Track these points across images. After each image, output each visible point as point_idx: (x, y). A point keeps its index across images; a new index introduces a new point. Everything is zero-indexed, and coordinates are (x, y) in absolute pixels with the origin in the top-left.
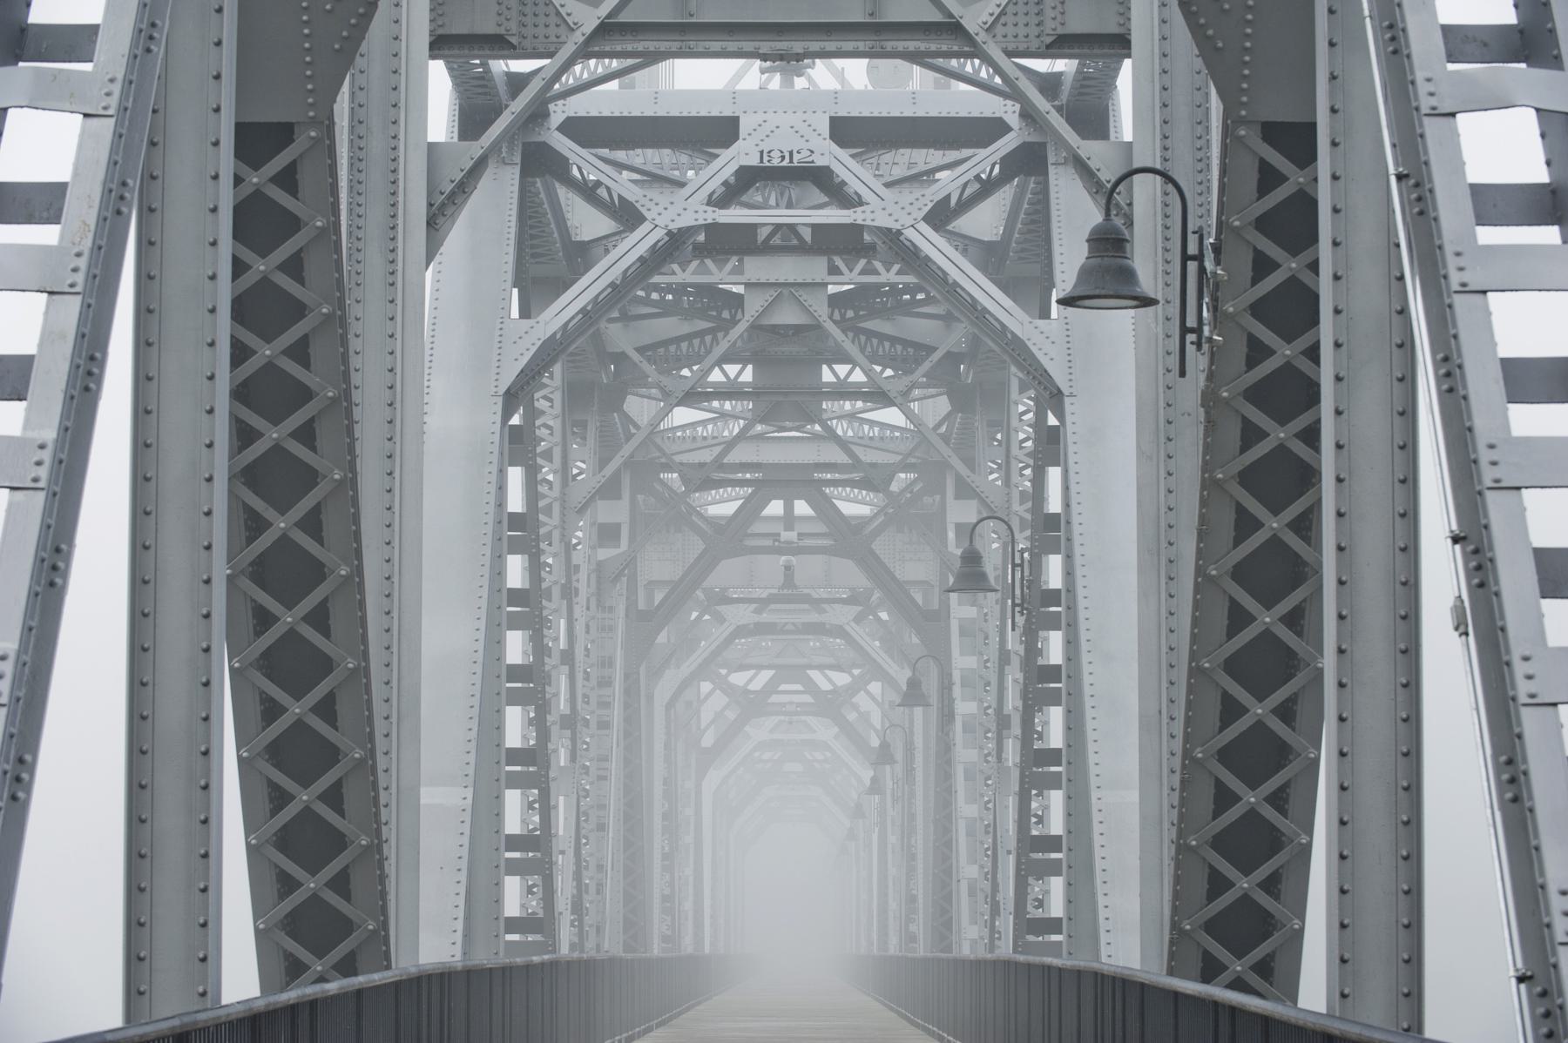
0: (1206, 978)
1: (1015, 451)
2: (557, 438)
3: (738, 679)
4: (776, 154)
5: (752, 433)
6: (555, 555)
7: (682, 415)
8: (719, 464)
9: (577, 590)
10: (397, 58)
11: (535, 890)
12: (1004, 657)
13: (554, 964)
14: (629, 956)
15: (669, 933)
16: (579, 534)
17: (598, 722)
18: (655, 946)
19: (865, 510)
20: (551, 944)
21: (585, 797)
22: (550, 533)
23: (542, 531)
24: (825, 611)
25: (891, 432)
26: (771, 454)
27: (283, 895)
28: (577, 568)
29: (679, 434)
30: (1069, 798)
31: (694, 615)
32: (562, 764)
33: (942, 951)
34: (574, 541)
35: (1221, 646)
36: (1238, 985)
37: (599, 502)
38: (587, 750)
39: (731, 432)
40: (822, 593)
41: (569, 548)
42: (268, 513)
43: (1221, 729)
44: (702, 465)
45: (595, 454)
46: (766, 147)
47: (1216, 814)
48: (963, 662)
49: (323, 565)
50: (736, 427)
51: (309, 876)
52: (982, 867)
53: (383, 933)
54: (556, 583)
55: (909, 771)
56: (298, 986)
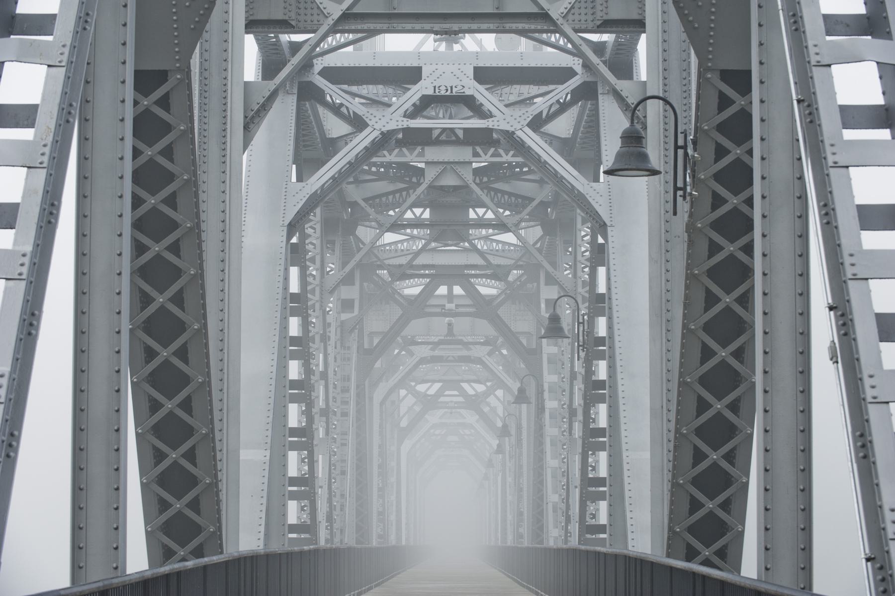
0: (689, 559)
1: (579, 258)
2: (318, 250)
3: (421, 388)
4: (443, 88)
5: (429, 247)
6: (317, 317)
7: (390, 237)
8: (410, 265)
9: (329, 337)
11: (305, 508)
12: (573, 376)
13: (316, 551)
14: (359, 546)
15: (382, 533)
16: (331, 305)
17: (342, 413)
18: (374, 541)
19: (494, 292)
20: (315, 540)
21: (334, 456)
22: (314, 305)
23: (310, 303)
24: (471, 349)
25: (509, 247)
27: (161, 512)
28: (329, 324)
29: (388, 248)
31: (396, 351)
32: (321, 437)
34: (328, 309)
36: (707, 563)
37: (342, 287)
38: (335, 428)
40: (469, 339)
41: (325, 313)
42: (153, 293)
43: (697, 417)
44: (401, 266)
45: (340, 259)
46: (437, 84)
47: (695, 465)
48: (549, 378)
50: (420, 244)
52: (560, 495)
54: (317, 333)
55: (519, 441)
56: (170, 564)
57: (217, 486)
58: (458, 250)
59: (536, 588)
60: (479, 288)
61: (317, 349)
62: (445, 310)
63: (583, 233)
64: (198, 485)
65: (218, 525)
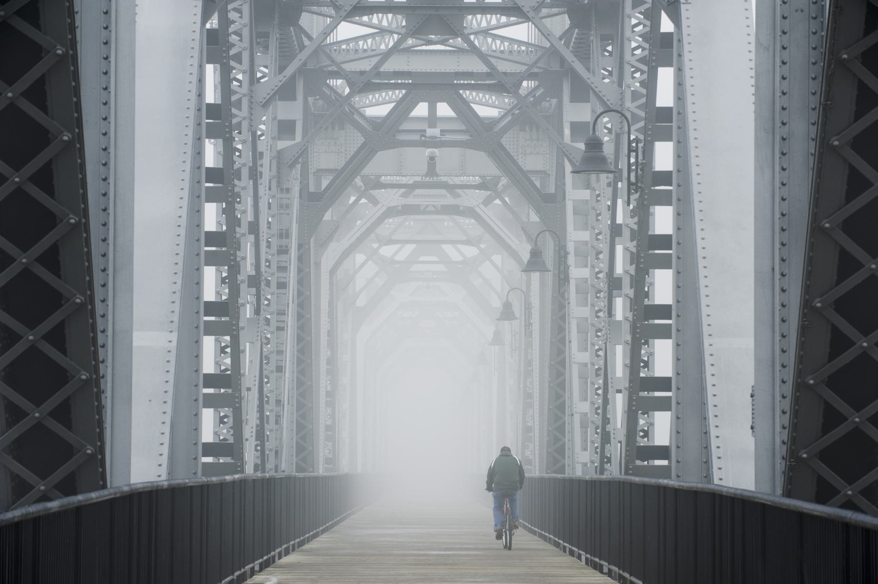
0: (820, 499)
1: (628, 57)
2: (246, 44)
3: (387, 251)
5: (404, 46)
6: (244, 142)
7: (346, 30)
8: (376, 71)
9: (261, 173)
10: (106, 122)
11: (226, 420)
12: (616, 230)
13: (243, 482)
14: (301, 475)
15: (330, 456)
16: (263, 127)
17: (278, 283)
18: (321, 467)
19: (494, 113)
20: (239, 467)
21: (267, 344)
22: (240, 123)
23: (235, 121)
24: (459, 196)
25: (519, 46)
26: (418, 65)
28: (261, 154)
29: (344, 47)
30: (678, 345)
31: (352, 199)
32: (248, 316)
33: (554, 472)
34: (259, 133)
35: (840, 209)
36: (849, 505)
37: (279, 103)
38: (268, 305)
39: (387, 46)
40: (458, 180)
41: (255, 138)
43: (838, 282)
44: (362, 73)
45: (276, 61)
47: (832, 357)
48: (576, 236)
49: (48, 132)
50: (391, 41)
51: (33, 406)
52: (593, 403)
53: (100, 457)
54: (244, 165)
55: (528, 325)
56: (22, 505)
57: (98, 385)
58: (450, 51)
59: (532, 525)
60: (476, 108)
61: (244, 188)
62: (425, 137)
63: (634, 21)
64: (68, 382)
65: (99, 444)
